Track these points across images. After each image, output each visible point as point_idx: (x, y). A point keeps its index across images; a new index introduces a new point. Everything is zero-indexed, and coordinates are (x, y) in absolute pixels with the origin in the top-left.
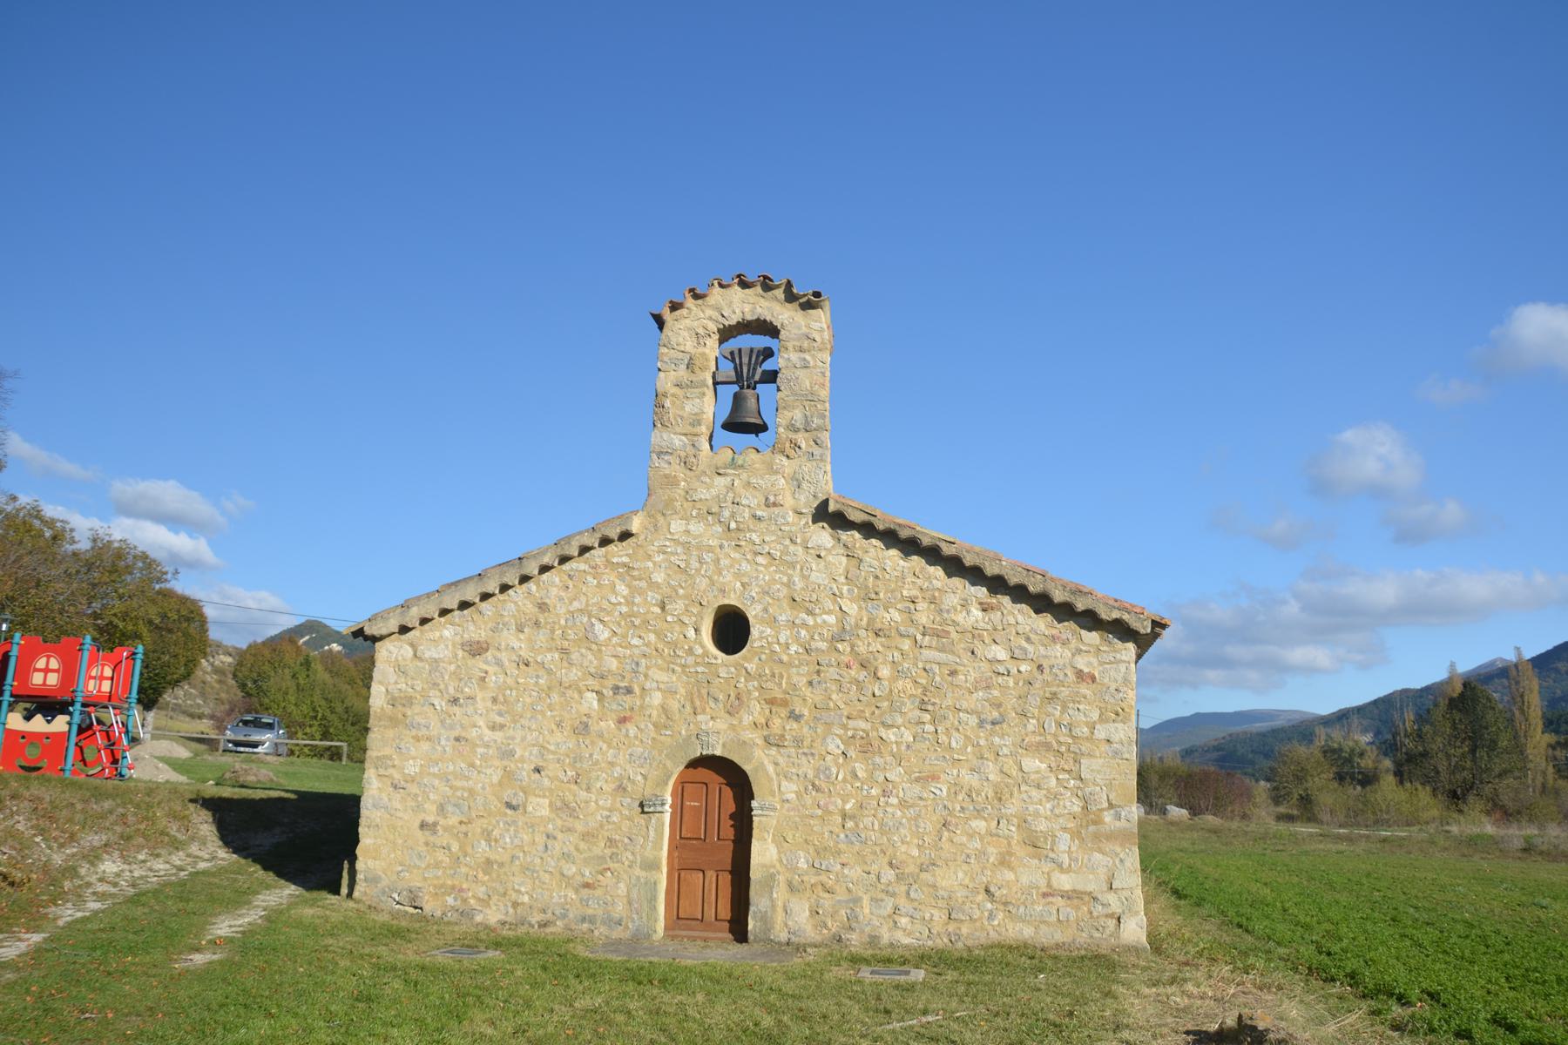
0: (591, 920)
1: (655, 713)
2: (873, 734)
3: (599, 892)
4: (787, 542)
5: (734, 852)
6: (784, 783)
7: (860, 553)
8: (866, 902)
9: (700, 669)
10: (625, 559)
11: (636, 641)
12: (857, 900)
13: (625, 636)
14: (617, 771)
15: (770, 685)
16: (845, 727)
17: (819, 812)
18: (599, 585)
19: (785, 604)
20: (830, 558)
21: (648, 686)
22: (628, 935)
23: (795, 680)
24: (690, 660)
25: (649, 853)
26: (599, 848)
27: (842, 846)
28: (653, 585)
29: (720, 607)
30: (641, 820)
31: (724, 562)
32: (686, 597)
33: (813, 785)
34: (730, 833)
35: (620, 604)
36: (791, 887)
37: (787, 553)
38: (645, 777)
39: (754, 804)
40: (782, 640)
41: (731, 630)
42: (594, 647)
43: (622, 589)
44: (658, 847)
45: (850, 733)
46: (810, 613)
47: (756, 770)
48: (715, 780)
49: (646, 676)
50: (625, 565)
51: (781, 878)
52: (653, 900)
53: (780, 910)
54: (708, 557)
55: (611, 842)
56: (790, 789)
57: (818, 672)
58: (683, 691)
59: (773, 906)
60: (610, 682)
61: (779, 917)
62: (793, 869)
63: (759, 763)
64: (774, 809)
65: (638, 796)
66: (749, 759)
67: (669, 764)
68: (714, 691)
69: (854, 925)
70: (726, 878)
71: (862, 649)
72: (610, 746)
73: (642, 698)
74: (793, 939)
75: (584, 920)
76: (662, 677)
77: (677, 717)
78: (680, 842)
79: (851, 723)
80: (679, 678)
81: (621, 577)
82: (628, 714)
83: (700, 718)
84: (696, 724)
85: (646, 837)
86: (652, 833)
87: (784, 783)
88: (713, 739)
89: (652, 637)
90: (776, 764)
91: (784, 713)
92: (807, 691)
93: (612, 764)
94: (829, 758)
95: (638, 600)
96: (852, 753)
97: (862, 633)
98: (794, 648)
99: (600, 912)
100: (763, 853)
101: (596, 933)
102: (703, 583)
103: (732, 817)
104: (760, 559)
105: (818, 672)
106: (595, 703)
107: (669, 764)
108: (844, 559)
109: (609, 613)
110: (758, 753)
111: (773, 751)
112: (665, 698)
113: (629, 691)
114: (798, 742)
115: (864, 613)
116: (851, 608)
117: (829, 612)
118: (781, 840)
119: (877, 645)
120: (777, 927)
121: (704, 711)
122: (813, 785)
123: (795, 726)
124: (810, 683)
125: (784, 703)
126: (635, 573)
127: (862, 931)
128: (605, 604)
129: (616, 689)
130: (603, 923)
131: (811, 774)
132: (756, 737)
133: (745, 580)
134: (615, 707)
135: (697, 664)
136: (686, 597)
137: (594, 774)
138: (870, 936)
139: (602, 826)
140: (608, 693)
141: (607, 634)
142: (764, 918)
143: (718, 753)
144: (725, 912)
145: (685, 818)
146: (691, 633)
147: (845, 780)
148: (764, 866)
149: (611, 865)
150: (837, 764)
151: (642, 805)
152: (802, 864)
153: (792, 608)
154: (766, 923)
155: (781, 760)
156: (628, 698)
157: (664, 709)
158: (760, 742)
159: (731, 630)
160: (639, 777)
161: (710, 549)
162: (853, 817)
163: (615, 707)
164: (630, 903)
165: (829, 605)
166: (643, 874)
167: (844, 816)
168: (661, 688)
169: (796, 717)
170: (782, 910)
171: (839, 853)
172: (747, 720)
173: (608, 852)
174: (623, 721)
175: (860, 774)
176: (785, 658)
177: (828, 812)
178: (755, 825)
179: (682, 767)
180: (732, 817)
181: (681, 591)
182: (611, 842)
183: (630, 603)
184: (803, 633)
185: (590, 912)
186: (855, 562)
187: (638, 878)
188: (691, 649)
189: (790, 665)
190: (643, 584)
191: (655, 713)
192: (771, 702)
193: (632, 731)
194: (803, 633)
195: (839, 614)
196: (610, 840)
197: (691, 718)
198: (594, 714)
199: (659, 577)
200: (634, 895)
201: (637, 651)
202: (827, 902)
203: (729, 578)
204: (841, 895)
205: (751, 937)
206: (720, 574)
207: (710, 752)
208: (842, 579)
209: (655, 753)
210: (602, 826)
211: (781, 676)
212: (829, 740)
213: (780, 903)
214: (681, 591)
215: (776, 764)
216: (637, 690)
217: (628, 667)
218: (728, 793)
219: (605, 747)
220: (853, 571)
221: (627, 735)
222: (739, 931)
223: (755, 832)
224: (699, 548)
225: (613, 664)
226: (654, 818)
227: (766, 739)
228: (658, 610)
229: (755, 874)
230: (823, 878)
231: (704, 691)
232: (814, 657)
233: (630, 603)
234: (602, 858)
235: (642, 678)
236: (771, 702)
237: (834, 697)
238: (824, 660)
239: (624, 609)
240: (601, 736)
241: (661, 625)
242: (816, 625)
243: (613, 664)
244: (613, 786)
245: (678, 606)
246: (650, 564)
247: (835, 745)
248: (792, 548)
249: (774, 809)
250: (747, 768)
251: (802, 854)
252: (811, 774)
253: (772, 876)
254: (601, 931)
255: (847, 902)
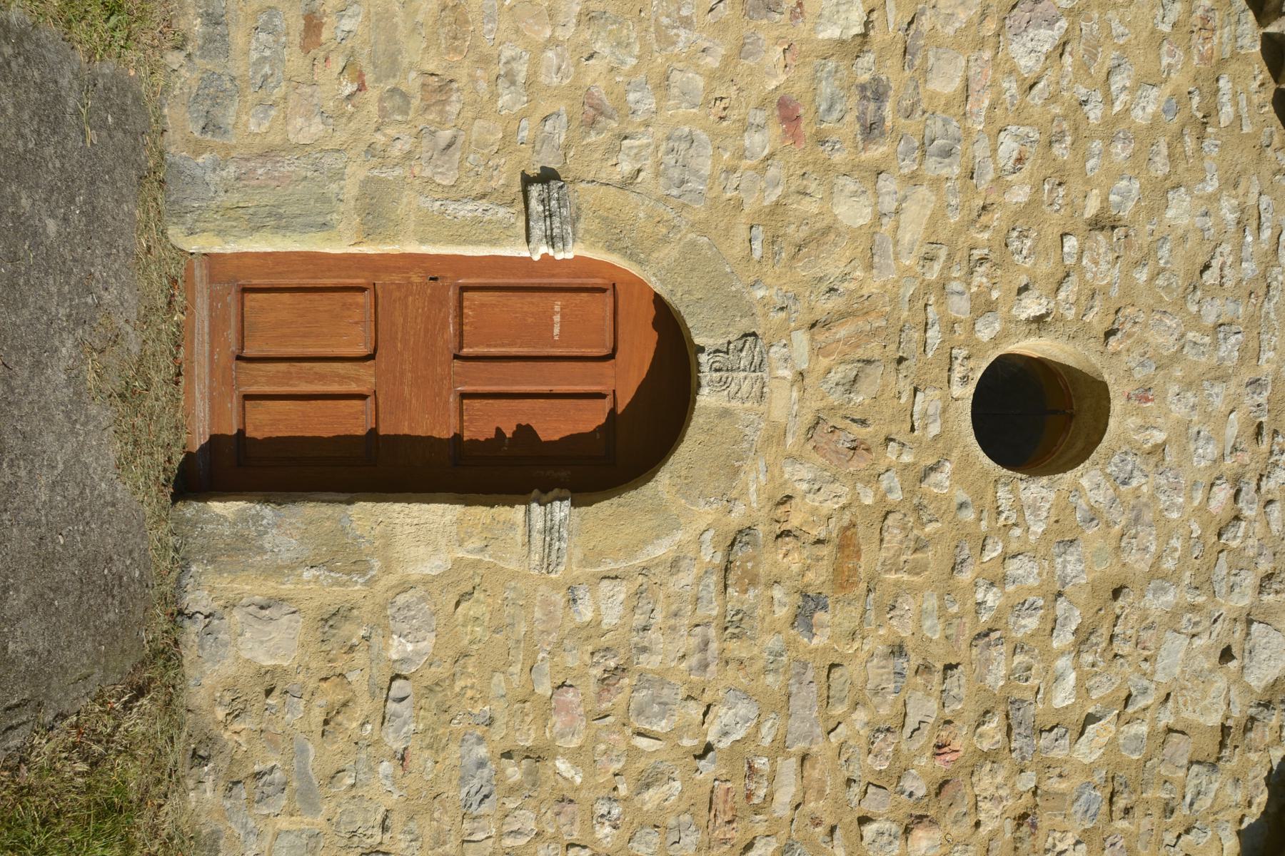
0: (216, 43)
1: (810, 206)
2: (760, 825)
3: (295, 61)
4: (1265, 566)
5: (429, 442)
6: (621, 591)
7: (1233, 762)
8: (306, 822)
9: (934, 335)
10: (1226, 114)
11: (1008, 147)
12: (308, 799)
13: (1021, 115)
14: (643, 101)
15: (894, 536)
16: (780, 748)
17: (545, 689)
18: (1157, 40)
19: (1107, 568)
20: (1220, 683)
21: (888, 184)
22: (176, 151)
23: (907, 605)
24: (960, 307)
25: (410, 203)
26: (420, 58)
27: (454, 752)
28: (1160, 192)
29: (1103, 387)
30: (506, 176)
31: (1219, 396)
32: (1128, 290)
33: (620, 670)
34: (484, 423)
35: (1109, 100)
36: (332, 619)
37: (1236, 569)
38: (628, 183)
39: (561, 510)
40: (1013, 567)
41: (1033, 415)
42: (990, 26)
43: (1148, 107)
44: (431, 226)
45: (761, 763)
46: (1083, 638)
47: (659, 508)
48: (626, 378)
49: (914, 179)
50: (1209, 115)
51: (357, 589)
52: (278, 221)
53: (270, 588)
54: (1229, 348)
55: (439, 88)
56: (607, 607)
57: (925, 669)
58: (872, 287)
59: (277, 571)
60: (892, 73)
61: (252, 587)
62: (383, 625)
63: (673, 516)
64: (548, 566)
65: (572, 167)
66: (687, 488)
67: (669, 253)
68: (874, 381)
69: (242, 792)
70: (351, 421)
71: (986, 782)
72: (712, 76)
73: (853, 170)
74: (192, 629)
75: (213, 19)
76: (912, 230)
77: (803, 271)
78: (459, 285)
79: (788, 766)
80: (906, 273)
81: (1177, 102)
82: (806, 128)
83: (801, 340)
84: (785, 331)
85: (455, 193)
86: (466, 210)
87: (621, 591)
88: (743, 381)
89: (1019, 195)
90: (675, 565)
91: (817, 578)
92: (875, 643)
93: (663, 84)
94: (695, 710)
95: (1120, 151)
96: (708, 768)
97: (1027, 781)
98: (992, 598)
99: (238, 67)
100: (424, 536)
101: (175, 59)
102: (1162, 339)
103: (525, 432)
104: (1222, 494)
105: (925, 669)
106: (831, 32)
107: (669, 253)
108: (1215, 720)
109: (1084, 67)
110: (706, 513)
111: (711, 555)
112: (854, 234)
113: (871, 130)
114: (734, 625)
115: (1078, 780)
116: (1089, 749)
117: (1082, 689)
118: (463, 587)
119: (994, 819)
120: (223, 582)
121: (818, 351)
122: (620, 670)
123: (782, 613)
124: (898, 650)
125: (843, 580)
126: (1190, 143)
127: (225, 814)
128: (1108, 57)
129: (876, 92)
130: (209, 79)
131: (650, 662)
132: (751, 505)
133: (1171, 457)
134: (826, 89)
135: (951, 326)
136: (1128, 290)
137: (631, 32)
138: (215, 836)
139: (484, 61)
140: (865, 69)
141: (1027, 63)
142: (240, 548)
143: (706, 399)
144: (268, 423)
145: (514, 299)
146: (1032, 306)
147: (633, 753)
148: (388, 540)
149: (372, 94)
150: (677, 732)
151: (548, 176)
152: (398, 648)
153: (1094, 588)
154: (232, 550)
155: (685, 578)
156: (851, 127)
157: (824, 233)
158: (737, 517)
159: (1033, 415)
160: (626, 167)
161: (1250, 354)
162: (534, 780)
163: (826, 89)
164: (267, 154)
165: (1102, 690)
166: (351, 188)
167: (536, 756)
168: (886, 221)
169: (808, 608)
170: (271, 598)
171: (436, 746)
172: (798, 476)
173: (412, 82)
174: (788, 113)
175: (652, 797)
176: (966, 576)
177: (547, 710)
178: (502, 512)
179: (658, 289)
180: (525, 432)
181: (1142, 276)
182: (439, 88)
183: (1111, 129)
184: (1031, 623)
185: (238, 38)
186: (1210, 746)
187: (338, 175)
188: (990, 307)
189: (947, 592)
190: (1160, 167)
191: (810, 206)
192: (847, 543)
193: (758, 142)
194: (1031, 623)
195: (1077, 716)
196: (446, 86)
197: (801, 314)
198: (803, 28)
199: (1179, 211)
200: (290, 166)
201: (981, 150)
202: (298, 717)
203: (1178, 411)
204: (319, 757)
205: (190, 509)
206: (1189, 385)
207: (706, 376)
208: (1167, 718)
209: (700, 211)
210: (484, 61)
211: (916, 570)
212: (743, 709)
213: (287, 588)
214: (1142, 276)
215: (675, 565)
216: (876, 152)
217: (936, 127)
218: (590, 418)
219: (712, 62)
220: (1181, 748)
221: (746, 127)
222: (222, 468)
223: (481, 514)
224: (1254, 320)
225: (944, 84)
226: (509, 215)
227: (740, 537)
228: (1092, 208)
229: (366, 516)
230: (364, 706)
231: (873, 349)
232: (963, 653)
233: (1111, 129)
234: (392, 65)
235: (908, 167)
236: (847, 543)
237: (861, 716)
238: (958, 684)
239: (1095, 113)
240: (742, 50)
241: (1054, 219)
242: (1049, 656)
243: (944, 84)
244: (600, 90)
245: (1101, 264)
246: (1211, 187)
247: (730, 722)
248: (1249, 580)
249: (548, 566)
250: (664, 482)
251: (427, 645)
252: (650, 662)
253: (359, 565)
254: (184, 73)
255: (303, 774)
